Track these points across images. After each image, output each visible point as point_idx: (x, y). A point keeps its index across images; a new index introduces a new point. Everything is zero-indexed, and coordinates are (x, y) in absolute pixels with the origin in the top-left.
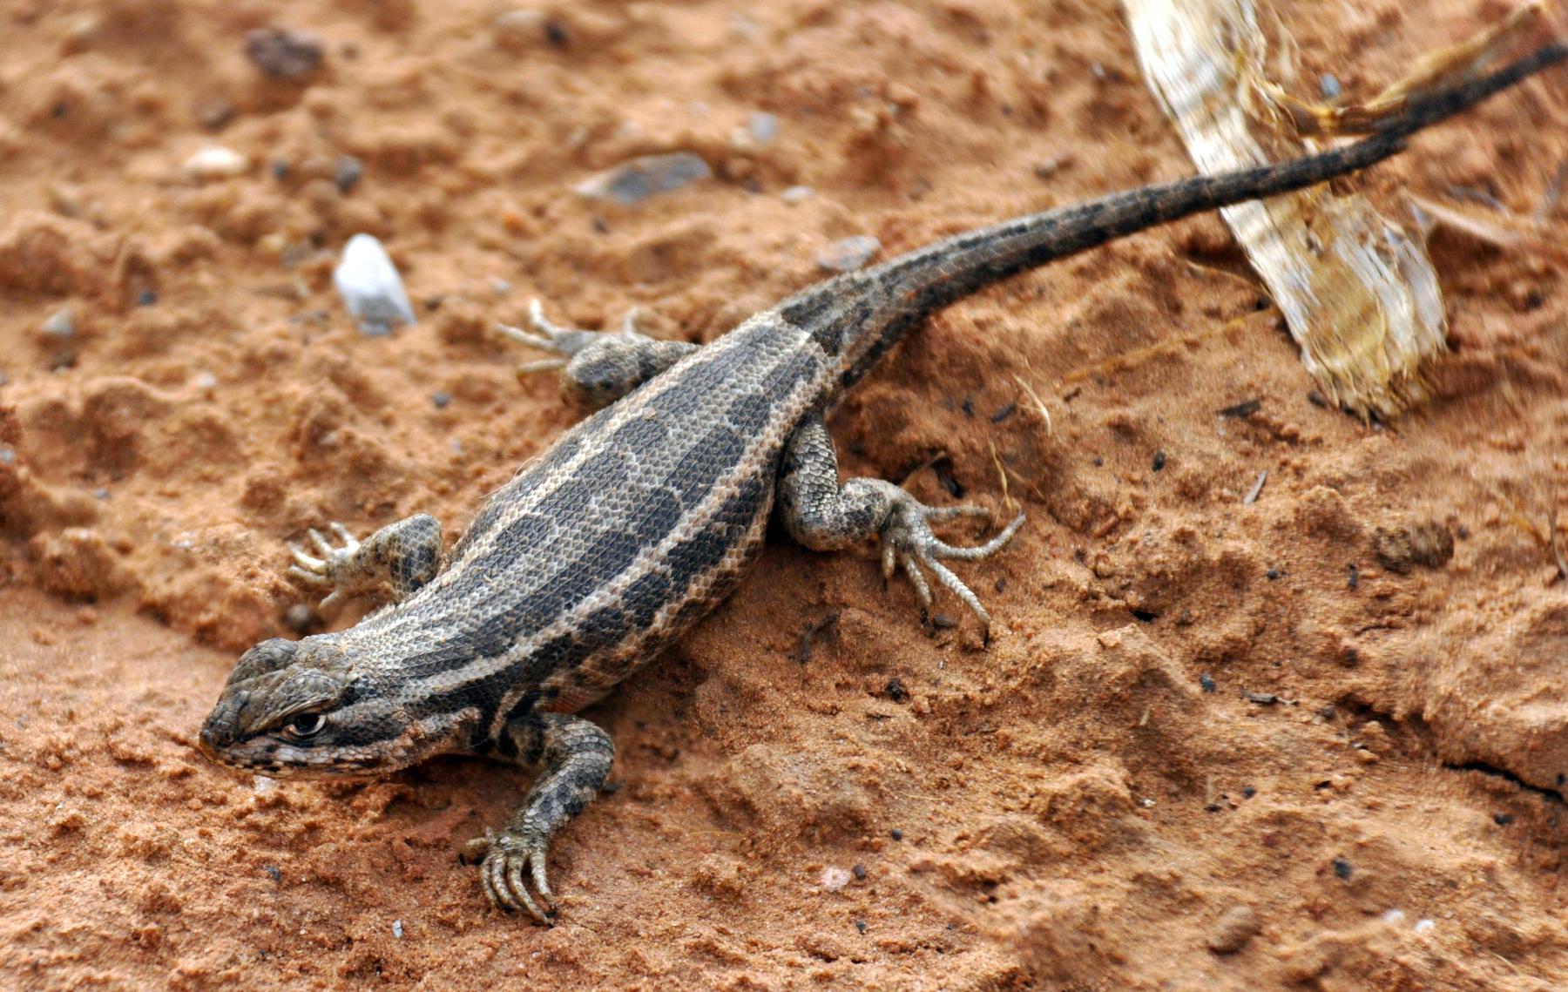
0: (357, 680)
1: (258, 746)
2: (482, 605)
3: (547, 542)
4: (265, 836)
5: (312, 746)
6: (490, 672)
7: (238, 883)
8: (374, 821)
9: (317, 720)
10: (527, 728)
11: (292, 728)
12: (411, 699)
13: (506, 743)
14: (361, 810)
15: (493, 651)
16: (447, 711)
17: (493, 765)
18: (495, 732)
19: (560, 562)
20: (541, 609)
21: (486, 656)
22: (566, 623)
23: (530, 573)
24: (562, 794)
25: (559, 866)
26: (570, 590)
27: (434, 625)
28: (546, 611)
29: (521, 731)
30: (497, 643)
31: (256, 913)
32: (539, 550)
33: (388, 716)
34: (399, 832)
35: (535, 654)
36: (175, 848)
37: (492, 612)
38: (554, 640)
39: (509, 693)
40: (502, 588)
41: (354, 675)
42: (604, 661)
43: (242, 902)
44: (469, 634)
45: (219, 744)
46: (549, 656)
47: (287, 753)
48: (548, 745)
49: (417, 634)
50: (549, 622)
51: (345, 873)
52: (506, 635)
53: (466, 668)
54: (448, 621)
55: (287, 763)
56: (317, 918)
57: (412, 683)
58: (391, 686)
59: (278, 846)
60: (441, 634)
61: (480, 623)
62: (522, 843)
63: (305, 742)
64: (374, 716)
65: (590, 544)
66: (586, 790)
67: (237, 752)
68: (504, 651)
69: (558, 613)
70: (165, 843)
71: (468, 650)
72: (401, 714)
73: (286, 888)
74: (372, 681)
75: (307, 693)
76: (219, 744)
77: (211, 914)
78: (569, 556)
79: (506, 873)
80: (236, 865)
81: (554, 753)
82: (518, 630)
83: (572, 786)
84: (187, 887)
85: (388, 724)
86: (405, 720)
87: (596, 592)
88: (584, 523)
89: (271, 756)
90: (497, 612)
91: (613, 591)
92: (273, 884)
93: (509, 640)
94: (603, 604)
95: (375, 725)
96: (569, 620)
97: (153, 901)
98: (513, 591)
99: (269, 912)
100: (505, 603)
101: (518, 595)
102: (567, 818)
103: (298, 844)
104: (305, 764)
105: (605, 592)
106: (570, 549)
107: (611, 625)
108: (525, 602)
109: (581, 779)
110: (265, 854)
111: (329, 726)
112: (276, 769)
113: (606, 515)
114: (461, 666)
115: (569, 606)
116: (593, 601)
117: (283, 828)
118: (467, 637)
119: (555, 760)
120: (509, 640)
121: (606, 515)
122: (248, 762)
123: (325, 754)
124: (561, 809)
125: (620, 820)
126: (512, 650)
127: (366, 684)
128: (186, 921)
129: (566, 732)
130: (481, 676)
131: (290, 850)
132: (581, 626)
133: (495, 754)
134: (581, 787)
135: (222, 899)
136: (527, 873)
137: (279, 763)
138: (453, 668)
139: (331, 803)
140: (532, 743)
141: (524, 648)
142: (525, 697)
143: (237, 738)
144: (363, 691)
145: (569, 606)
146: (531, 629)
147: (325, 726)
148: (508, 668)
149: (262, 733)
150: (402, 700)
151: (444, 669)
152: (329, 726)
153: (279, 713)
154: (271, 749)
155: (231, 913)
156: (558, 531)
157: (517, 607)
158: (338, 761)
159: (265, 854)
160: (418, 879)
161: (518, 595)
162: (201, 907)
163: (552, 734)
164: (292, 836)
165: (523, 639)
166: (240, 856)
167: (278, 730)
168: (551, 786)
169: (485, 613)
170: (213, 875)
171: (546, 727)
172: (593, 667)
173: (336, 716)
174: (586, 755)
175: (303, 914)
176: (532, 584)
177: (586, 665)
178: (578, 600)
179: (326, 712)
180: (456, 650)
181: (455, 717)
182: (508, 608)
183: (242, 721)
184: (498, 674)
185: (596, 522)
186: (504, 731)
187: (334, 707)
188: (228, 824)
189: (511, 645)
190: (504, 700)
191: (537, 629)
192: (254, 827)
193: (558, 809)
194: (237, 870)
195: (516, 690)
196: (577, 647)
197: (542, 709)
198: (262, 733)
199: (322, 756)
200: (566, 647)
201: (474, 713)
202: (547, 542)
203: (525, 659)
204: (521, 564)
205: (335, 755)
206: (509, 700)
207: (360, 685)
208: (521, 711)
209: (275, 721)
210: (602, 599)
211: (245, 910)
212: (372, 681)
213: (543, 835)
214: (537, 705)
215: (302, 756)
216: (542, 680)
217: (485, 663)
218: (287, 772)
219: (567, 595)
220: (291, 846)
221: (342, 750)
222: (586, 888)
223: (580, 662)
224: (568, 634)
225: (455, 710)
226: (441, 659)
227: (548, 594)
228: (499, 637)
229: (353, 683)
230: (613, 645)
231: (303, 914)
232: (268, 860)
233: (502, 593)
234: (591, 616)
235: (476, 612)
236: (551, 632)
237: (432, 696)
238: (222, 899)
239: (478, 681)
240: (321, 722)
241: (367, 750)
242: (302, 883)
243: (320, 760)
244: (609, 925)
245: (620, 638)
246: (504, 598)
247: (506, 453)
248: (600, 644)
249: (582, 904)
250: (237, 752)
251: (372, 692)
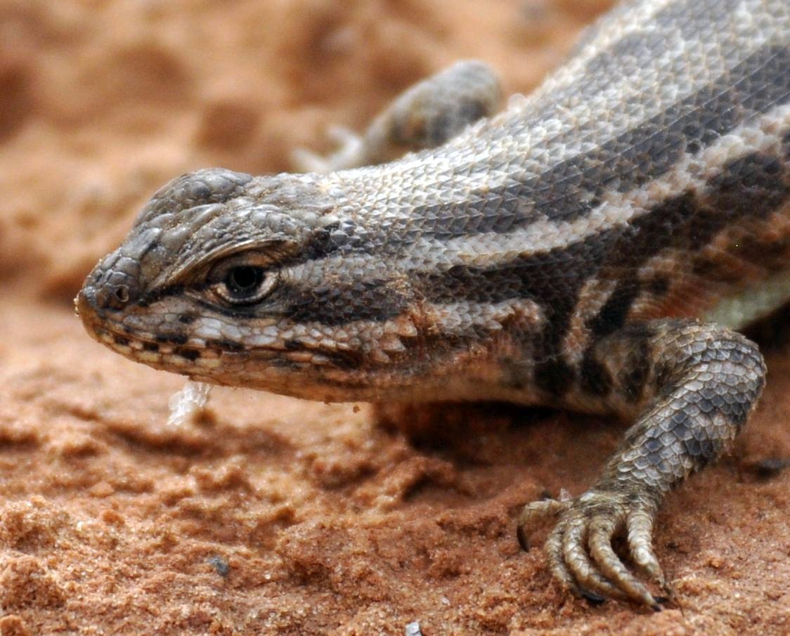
0: (336, 226)
1: (167, 311)
2: (549, 143)
3: (665, 61)
4: (207, 524)
5: (252, 316)
6: (561, 242)
7: (158, 575)
8: (388, 508)
9: (261, 279)
10: (624, 342)
11: (222, 289)
12: (420, 266)
13: (594, 377)
14: (367, 501)
15: (564, 210)
16: (482, 300)
17: (581, 423)
18: (573, 351)
19: (682, 86)
20: (647, 151)
21: (553, 218)
22: (687, 175)
23: (633, 100)
24: (679, 425)
25: (671, 545)
26: (697, 124)
27: (471, 170)
28: (655, 154)
29: (614, 349)
30: (570, 200)
31: (185, 610)
32: (650, 71)
33: (380, 283)
34: (424, 517)
35: (635, 221)
36: (62, 532)
37: (564, 152)
38: (669, 201)
39: (592, 282)
40: (585, 120)
41: (331, 218)
42: (747, 240)
43: (165, 599)
44: (525, 182)
45: (106, 306)
46: (657, 227)
47: (211, 327)
48: (656, 358)
49: (443, 179)
50: (659, 172)
51: (330, 557)
52: (587, 186)
53: (520, 233)
54: (493, 165)
55: (212, 344)
56: (286, 622)
57: (425, 242)
58: (392, 241)
59: (232, 540)
60: (484, 181)
61: (545, 168)
62: (615, 499)
63: (242, 310)
64: (357, 279)
65: (734, 62)
66: (718, 421)
67: (134, 321)
68: (583, 211)
69: (675, 158)
70: (45, 523)
71: (525, 206)
72: (403, 286)
73: (239, 588)
74: (359, 229)
75: (251, 228)
76: (106, 306)
77: (110, 608)
78: (698, 77)
79: (586, 546)
80: (158, 555)
81: (665, 370)
82: (607, 181)
83: (693, 413)
84: (77, 577)
85: (380, 297)
86: (407, 294)
87: (741, 128)
88: (726, 35)
89: (187, 329)
90: (575, 152)
91: (768, 129)
92: (218, 580)
93: (590, 196)
94: (752, 148)
95: (357, 293)
96: (693, 169)
97: (20, 588)
98: (602, 124)
99: (207, 609)
100: (589, 139)
101: (611, 128)
102: (687, 464)
103: (260, 537)
104: (238, 347)
105: (756, 130)
106: (699, 69)
107: (759, 181)
108: (620, 139)
109: (709, 405)
110: (206, 544)
111: (282, 288)
112: (193, 354)
113: (763, 25)
114: (511, 229)
115: (693, 149)
116: (735, 143)
117: (239, 514)
118: (522, 188)
119: (667, 380)
120: (590, 196)
121: (763, 25)
122: (150, 336)
123: (273, 331)
124: (677, 449)
125: (780, 498)
126: (596, 212)
127: (350, 232)
128: (72, 616)
129: (683, 338)
130: (545, 247)
131: (250, 545)
132: (712, 181)
133: (575, 397)
134: (708, 415)
135: (135, 591)
136: (620, 543)
137: (199, 343)
138: (495, 229)
139: (322, 495)
140: (633, 360)
141: (617, 211)
142: (617, 292)
143: (134, 297)
144: (343, 240)
145: (693, 149)
146: (630, 180)
147: (275, 289)
148: (589, 240)
149: (173, 290)
150: (406, 264)
151: (481, 229)
152: (282, 288)
153: (204, 255)
154: (187, 318)
155: (145, 610)
156: (682, 45)
157: (607, 146)
158: (294, 345)
159: (206, 544)
160: (450, 573)
161: (611, 128)
162: (98, 598)
163: (663, 340)
164: (252, 525)
165: (615, 194)
166: (168, 544)
167: (199, 287)
168: (663, 414)
169: (554, 153)
170: (120, 565)
171: (652, 334)
172: (730, 249)
173: (295, 274)
174: (717, 368)
175: (263, 617)
176: (634, 114)
177: (718, 245)
178: (708, 140)
179: (277, 266)
180: (503, 204)
181: (501, 310)
182: (593, 146)
183: (146, 270)
184: (573, 248)
185: (746, 33)
186: (589, 353)
187: (294, 258)
188: (152, 511)
189: (595, 203)
190: (584, 293)
191: (640, 181)
192: (194, 513)
193: (672, 450)
194: (160, 562)
195: (604, 276)
196: (703, 215)
197: (648, 314)
198: (173, 290)
199: (267, 334)
200: (685, 213)
201: (534, 312)
202: (665, 61)
203: (618, 227)
204: (617, 93)
205: (288, 335)
206: (592, 296)
207: (339, 232)
208: (610, 320)
209: (195, 269)
210: (750, 140)
211: (172, 607)
212: (359, 229)
213: (649, 489)
214: (637, 307)
215: (235, 333)
216: (642, 263)
217: (552, 228)
218: (210, 361)
219: (690, 132)
220: (251, 539)
221: (301, 329)
222: (718, 570)
223: (707, 239)
224: (690, 193)
225: (496, 300)
226: (476, 213)
227: (659, 128)
228: (574, 189)
229: (329, 227)
230: (764, 215)
231: (263, 617)
232: (212, 553)
233: (584, 127)
234: (730, 165)
235: (539, 152)
236: (663, 188)
237: (457, 269)
238: (135, 591)
239: (540, 255)
240: (269, 282)
241: (343, 334)
242: (264, 583)
243: (264, 341)
244: (755, 622)
245: (776, 204)
246: (586, 133)
247: (755, 594)
248: (742, 211)
249: (710, 590)
250: (134, 321)
251: (356, 244)
